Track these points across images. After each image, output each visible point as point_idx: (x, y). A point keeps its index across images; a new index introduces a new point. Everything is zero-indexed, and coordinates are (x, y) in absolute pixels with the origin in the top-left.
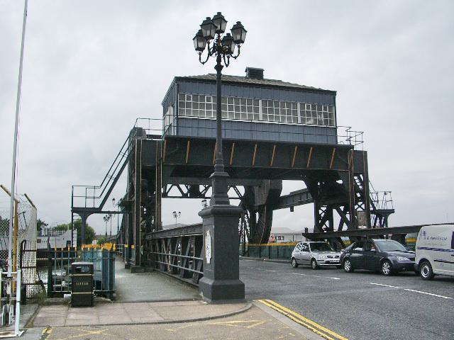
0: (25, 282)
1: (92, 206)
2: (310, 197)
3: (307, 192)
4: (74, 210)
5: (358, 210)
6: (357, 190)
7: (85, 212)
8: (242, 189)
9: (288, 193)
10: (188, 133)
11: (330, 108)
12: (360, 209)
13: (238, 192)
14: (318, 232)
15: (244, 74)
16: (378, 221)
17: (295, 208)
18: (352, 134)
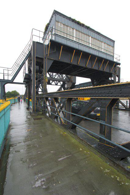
8: (62, 83)
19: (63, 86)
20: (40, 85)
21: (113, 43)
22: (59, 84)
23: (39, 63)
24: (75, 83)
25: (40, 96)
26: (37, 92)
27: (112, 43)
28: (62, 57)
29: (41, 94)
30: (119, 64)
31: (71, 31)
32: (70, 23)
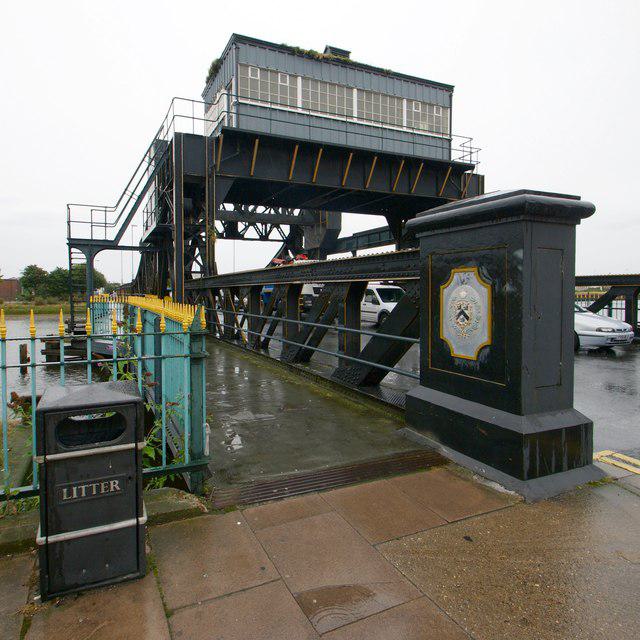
0: (169, 607)
1: (103, 238)
4: (73, 243)
7: (92, 247)
8: (286, 229)
10: (251, 125)
13: (281, 232)
19: (291, 243)
20: (197, 250)
21: (447, 94)
22: (275, 234)
23: (194, 190)
24: (338, 231)
25: (195, 286)
26: (189, 274)
27: (442, 95)
28: (254, 168)
29: (196, 280)
30: (472, 167)
31: (288, 84)
32: (284, 58)
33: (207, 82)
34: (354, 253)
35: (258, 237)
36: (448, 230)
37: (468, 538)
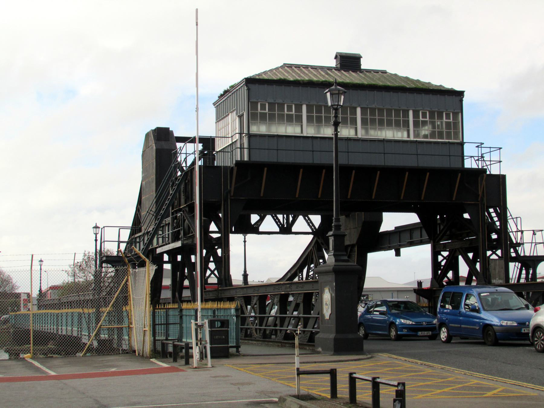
2: (425, 237)
3: (421, 228)
5: (491, 257)
6: (491, 228)
9: (391, 228)
11: (455, 115)
12: (494, 257)
14: (383, 304)
15: (333, 63)
16: (524, 272)
17: (403, 250)
18: (484, 151)
22: (300, 224)
33: (219, 97)
34: (461, 326)
35: (277, 230)
36: (453, 397)
37: (45, 271)
